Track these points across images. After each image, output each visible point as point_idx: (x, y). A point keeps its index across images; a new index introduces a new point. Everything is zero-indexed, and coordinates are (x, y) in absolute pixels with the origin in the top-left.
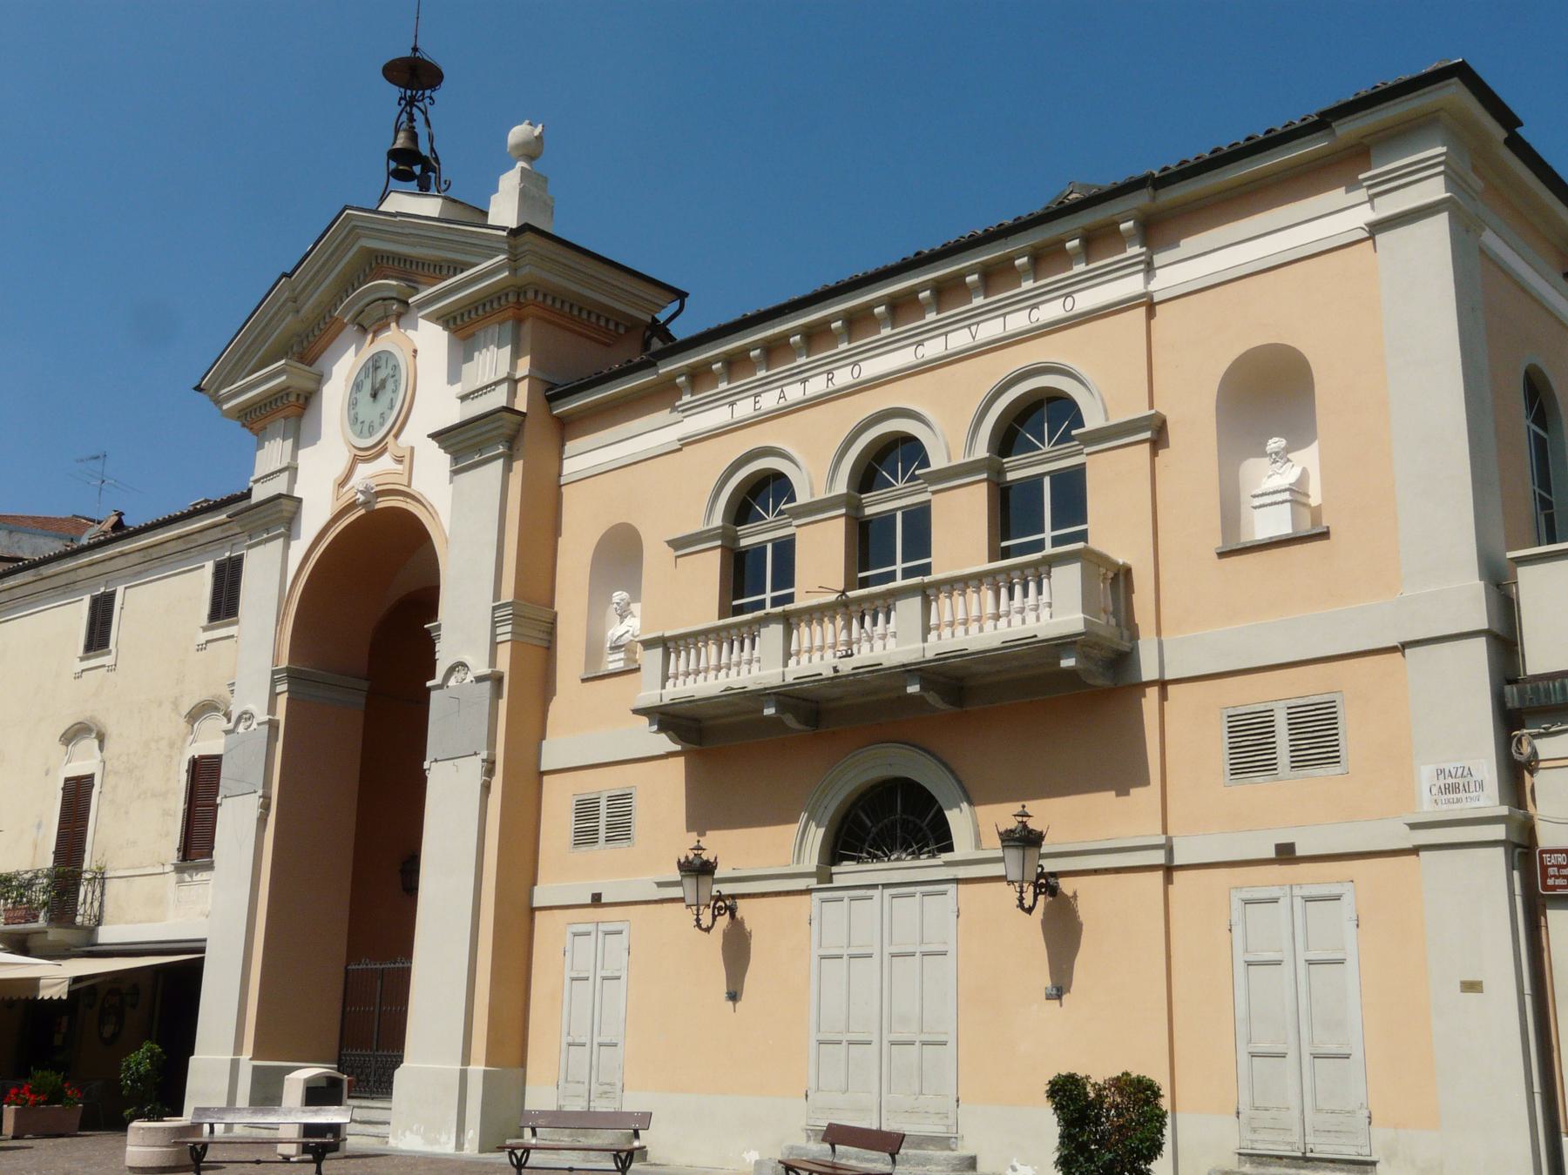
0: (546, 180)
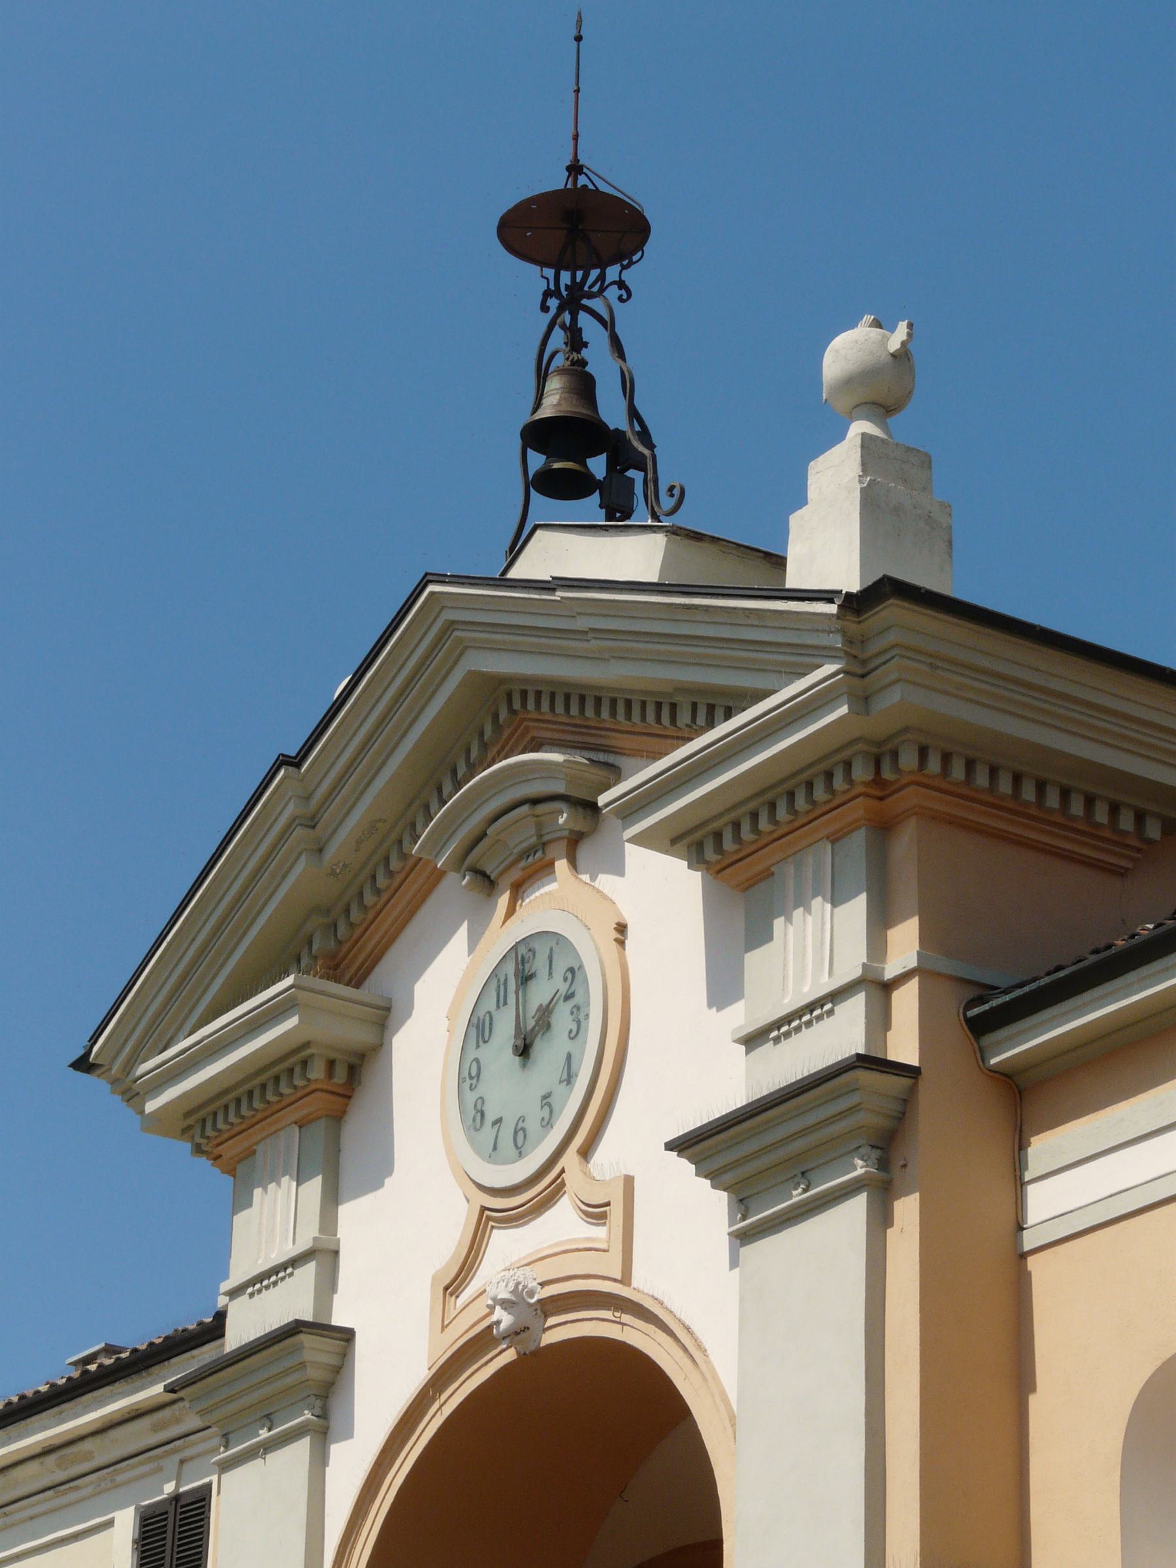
0: (926, 461)
